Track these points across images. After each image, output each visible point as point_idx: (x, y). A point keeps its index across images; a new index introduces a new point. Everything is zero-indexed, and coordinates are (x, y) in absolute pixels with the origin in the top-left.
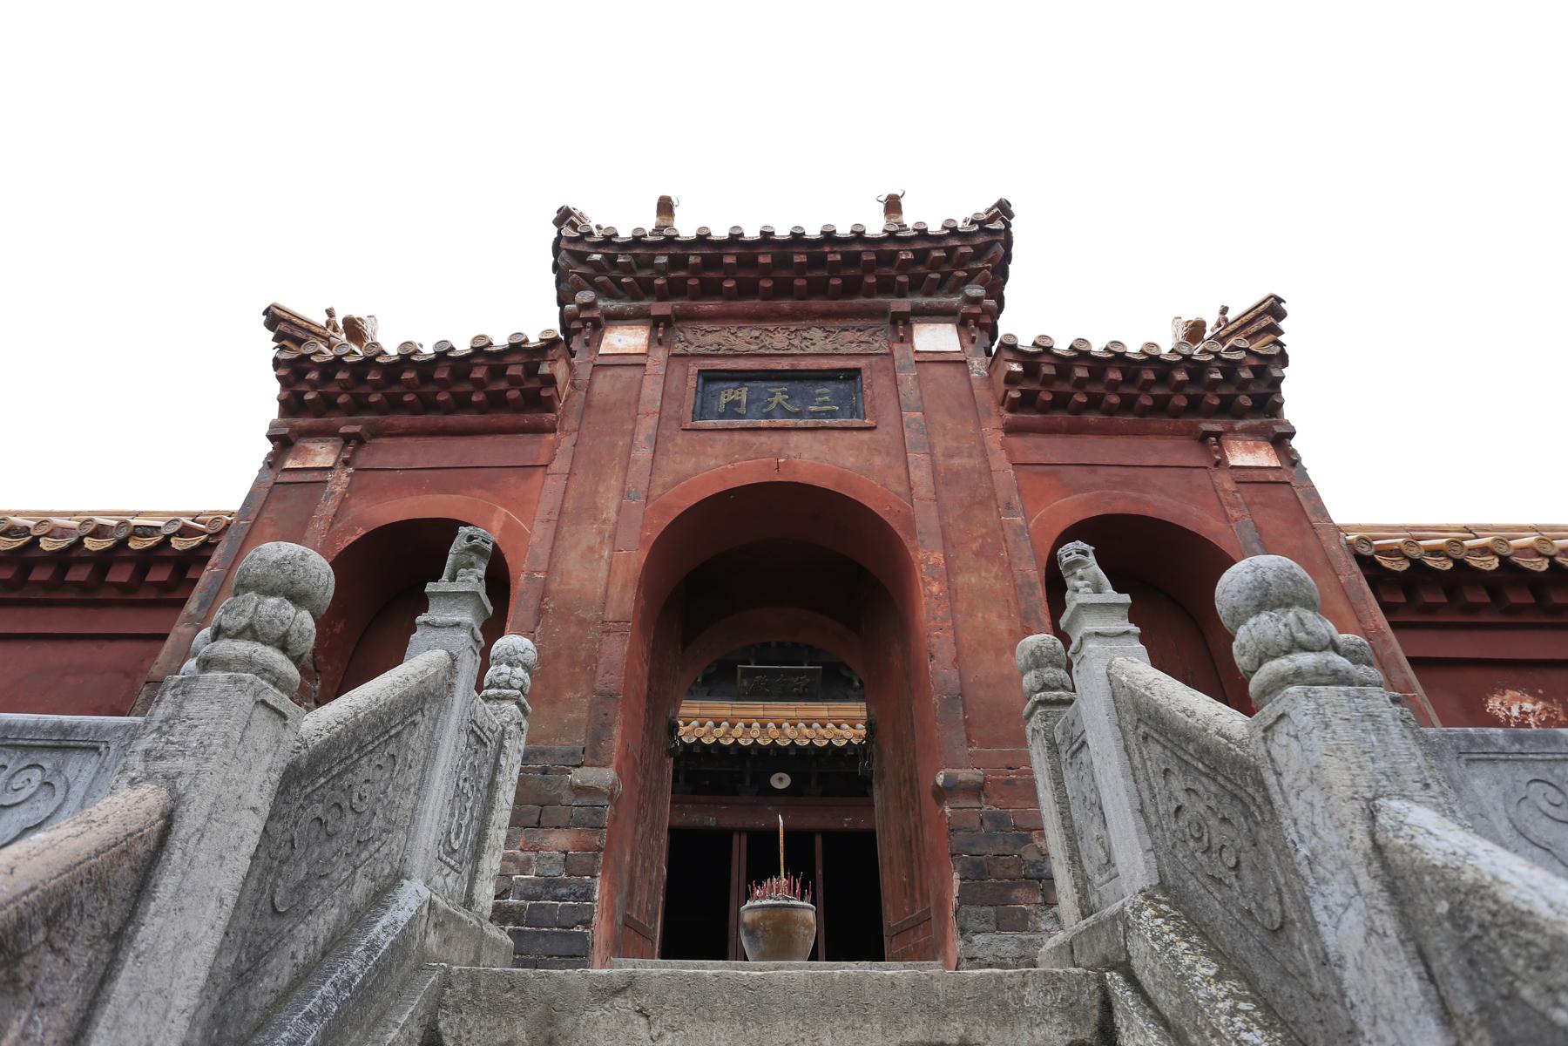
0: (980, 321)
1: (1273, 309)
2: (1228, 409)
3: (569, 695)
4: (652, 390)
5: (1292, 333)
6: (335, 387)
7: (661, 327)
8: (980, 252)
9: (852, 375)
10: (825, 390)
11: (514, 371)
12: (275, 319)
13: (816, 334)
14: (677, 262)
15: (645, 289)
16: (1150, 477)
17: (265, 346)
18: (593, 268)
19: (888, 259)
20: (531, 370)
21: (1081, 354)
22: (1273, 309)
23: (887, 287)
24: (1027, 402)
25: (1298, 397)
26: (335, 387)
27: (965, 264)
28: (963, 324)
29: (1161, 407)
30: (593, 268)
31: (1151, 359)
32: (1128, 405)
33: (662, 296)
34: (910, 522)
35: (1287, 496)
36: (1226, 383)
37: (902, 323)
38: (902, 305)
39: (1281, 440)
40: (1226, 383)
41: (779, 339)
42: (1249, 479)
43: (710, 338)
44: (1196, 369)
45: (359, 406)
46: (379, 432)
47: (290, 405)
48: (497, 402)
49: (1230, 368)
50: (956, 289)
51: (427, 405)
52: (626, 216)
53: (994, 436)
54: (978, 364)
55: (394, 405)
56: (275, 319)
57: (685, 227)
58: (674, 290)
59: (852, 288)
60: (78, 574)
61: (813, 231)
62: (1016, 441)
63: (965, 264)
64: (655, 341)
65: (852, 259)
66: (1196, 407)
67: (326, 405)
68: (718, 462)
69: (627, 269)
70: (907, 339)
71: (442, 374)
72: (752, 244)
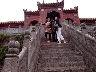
1: (78, 7)
2: (75, 12)
3: (48, 23)
4: (44, 13)
5: (78, 8)
6: (27, 14)
7: (44, 9)
8: (62, 3)
11: (35, 13)
12: (38, 2)
13: (53, 9)
14: (45, 5)
15: (43, 7)
16: (70, 16)
17: (37, 4)
18: (40, 6)
19: (57, 4)
21: (67, 10)
22: (78, 7)
23: (57, 6)
24: (64, 13)
25: (79, 11)
26: (27, 14)
28: (61, 8)
29: (71, 12)
30: (40, 6)
31: (69, 10)
32: (69, 13)
33: (44, 7)
35: (77, 16)
36: (75, 11)
37: (58, 8)
38: (58, 7)
39: (77, 14)
40: (75, 11)
42: (75, 16)
47: (25, 15)
48: (36, 14)
49: (75, 10)
51: (33, 14)
52: (41, 2)
55: (31, 14)
56: (24, 10)
57: (45, 3)
58: (45, 7)
59: (55, 6)
61: (52, 3)
62: (63, 15)
64: (44, 10)
65: (55, 5)
66: (73, 12)
67: (27, 15)
69: (42, 6)
71: (65, 11)
72: (49, 4)
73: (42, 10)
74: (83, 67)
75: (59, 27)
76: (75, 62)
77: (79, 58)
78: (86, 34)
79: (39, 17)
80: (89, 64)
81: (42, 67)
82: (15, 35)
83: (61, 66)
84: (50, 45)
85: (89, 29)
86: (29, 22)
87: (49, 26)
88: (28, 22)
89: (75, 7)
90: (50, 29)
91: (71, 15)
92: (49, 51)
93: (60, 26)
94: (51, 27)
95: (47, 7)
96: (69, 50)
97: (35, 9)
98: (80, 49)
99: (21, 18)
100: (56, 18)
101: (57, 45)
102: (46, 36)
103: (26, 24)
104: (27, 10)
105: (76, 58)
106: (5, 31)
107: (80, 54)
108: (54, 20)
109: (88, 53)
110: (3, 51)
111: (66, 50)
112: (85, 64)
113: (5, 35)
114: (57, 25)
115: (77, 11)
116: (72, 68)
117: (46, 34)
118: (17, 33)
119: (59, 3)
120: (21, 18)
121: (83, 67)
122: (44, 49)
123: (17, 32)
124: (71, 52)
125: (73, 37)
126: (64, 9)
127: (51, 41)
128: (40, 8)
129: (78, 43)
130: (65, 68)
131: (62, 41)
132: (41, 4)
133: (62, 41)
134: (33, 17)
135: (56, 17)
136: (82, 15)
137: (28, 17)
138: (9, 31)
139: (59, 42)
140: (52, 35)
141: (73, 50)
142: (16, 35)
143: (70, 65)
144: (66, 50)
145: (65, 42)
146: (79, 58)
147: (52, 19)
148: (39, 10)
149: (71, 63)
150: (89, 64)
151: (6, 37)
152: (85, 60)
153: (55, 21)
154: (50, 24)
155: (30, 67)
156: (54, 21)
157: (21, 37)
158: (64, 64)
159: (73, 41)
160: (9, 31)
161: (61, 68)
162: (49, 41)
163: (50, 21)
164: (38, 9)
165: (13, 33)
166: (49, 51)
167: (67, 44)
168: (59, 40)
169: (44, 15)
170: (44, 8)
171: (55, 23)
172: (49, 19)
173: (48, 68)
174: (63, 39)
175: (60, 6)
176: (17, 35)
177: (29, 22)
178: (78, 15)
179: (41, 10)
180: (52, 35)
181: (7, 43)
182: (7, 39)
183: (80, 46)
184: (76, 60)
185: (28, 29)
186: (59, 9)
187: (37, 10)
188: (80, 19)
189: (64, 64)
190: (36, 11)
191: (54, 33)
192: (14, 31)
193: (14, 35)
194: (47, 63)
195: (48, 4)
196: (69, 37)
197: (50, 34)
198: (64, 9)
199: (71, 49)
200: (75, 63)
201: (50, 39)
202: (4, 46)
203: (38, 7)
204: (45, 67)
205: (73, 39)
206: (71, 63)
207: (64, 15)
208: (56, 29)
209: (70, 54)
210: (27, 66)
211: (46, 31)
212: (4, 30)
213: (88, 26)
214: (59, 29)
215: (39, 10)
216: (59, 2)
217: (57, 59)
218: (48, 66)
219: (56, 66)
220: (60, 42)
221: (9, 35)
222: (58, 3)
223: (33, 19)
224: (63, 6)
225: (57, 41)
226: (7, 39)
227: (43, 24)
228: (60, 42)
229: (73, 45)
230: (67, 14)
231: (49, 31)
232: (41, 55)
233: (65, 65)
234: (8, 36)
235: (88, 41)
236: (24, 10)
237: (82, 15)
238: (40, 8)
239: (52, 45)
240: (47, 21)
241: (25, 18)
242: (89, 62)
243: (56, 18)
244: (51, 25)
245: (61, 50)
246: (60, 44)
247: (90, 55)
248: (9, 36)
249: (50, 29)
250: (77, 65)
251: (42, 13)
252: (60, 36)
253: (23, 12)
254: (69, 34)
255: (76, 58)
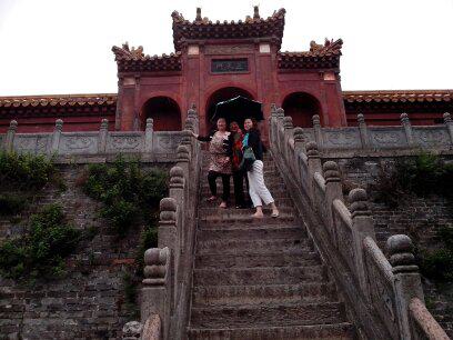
0: (278, 44)
1: (340, 42)
2: (327, 67)
3: (220, 137)
6: (130, 64)
7: (201, 47)
9: (246, 59)
10: (239, 64)
12: (174, 15)
15: (197, 36)
17: (170, 21)
18: (184, 32)
20: (176, 62)
24: (283, 66)
26: (130, 64)
27: (272, 28)
28: (271, 46)
29: (312, 67)
30: (184, 32)
33: (201, 38)
34: (256, 94)
36: (326, 59)
37: (257, 45)
38: (257, 40)
40: (326, 59)
41: (229, 50)
42: (329, 84)
43: (212, 50)
44: (319, 58)
45: (138, 70)
46: (143, 76)
47: (121, 70)
48: (169, 69)
49: (327, 58)
50: (271, 35)
53: (275, 74)
54: (274, 56)
55: (146, 69)
56: (115, 49)
58: (204, 36)
60: (87, 110)
63: (272, 28)
66: (320, 66)
67: (129, 70)
68: (217, 82)
70: (258, 50)
73: (193, 51)
74: (319, 299)
75: (259, 157)
76: (298, 286)
77: (313, 271)
78: (336, 197)
79: (181, 79)
80: (334, 292)
81: (205, 296)
82: (85, 160)
83: (258, 294)
84: (228, 221)
85: (374, 141)
86: (136, 104)
87: (224, 147)
88: (133, 100)
89: (327, 43)
90: (228, 159)
91: (312, 77)
92: (224, 247)
93: (260, 150)
94: (229, 154)
95: (212, 36)
96: (286, 244)
97: (160, 44)
98: (319, 243)
99: (103, 80)
100: (249, 123)
101: (250, 221)
102: (213, 187)
103: (126, 109)
104: (126, 47)
105: (302, 272)
106: (42, 143)
107: (317, 259)
108: (242, 128)
109: (335, 259)
110: (45, 227)
111: (277, 244)
112: (324, 290)
113: (47, 160)
114: (248, 154)
115: (338, 61)
116: (287, 302)
117: (213, 175)
118: (91, 152)
119: (263, 22)
120: (103, 80)
121: (319, 299)
122: (207, 235)
123: (93, 150)
124: (292, 249)
125: (304, 193)
126: (283, 50)
127: (228, 206)
128: (183, 39)
129: (314, 220)
130: (268, 301)
131: (267, 210)
132: (187, 23)
133: (267, 210)
134: (161, 78)
135: (249, 120)
136: (356, 77)
137: (131, 82)
138: (60, 145)
139: (255, 210)
140: (231, 180)
141: (297, 242)
142: (90, 160)
143: (282, 294)
144: (277, 244)
145: (276, 213)
146: (313, 271)
147: (234, 124)
148: (179, 53)
149: (287, 287)
150: (334, 292)
151: (49, 171)
152: (326, 278)
153: (244, 132)
154: (225, 141)
155: (179, 296)
156: (240, 131)
157: (112, 171)
158: (267, 289)
159: (301, 206)
160: (60, 145)
161: (259, 300)
162: (223, 205)
163: (227, 129)
164: (177, 47)
165: (78, 151)
166: (224, 247)
167: (283, 220)
168: (257, 202)
169: (201, 75)
170: (202, 42)
171: (245, 142)
172: (220, 122)
173: (222, 301)
174: (270, 199)
175: (269, 34)
176: (95, 160)
177: (139, 104)
178: (338, 79)
179: (186, 52)
180: (231, 180)
181: (57, 195)
182: (55, 177)
183: (320, 230)
184: (301, 277)
185: (134, 136)
186: (265, 49)
187: (173, 50)
188: (349, 94)
189: (267, 289)
190: (165, 57)
191: (241, 172)
192: (79, 143)
193: (81, 161)
194: (219, 288)
195: (218, 23)
196: (294, 190)
197: (226, 179)
198: (283, 50)
199: (293, 239)
200: (296, 287)
201: (226, 197)
202: (46, 206)
203: (176, 38)
204: (215, 297)
205: (305, 202)
206: (287, 287)
207: (283, 78)
208: (249, 165)
209: (287, 258)
210: (172, 296)
211: (213, 167)
212: (39, 137)
213: (373, 130)
214: (259, 164)
215: (179, 53)
216: (265, 18)
217: (248, 274)
218: (222, 295)
219: (244, 294)
220: (259, 209)
221: (63, 161)
222: (258, 21)
223: (156, 88)
224: (281, 35)
225: (246, 203)
226: (55, 177)
227: (199, 138)
228: (259, 209)
229: (302, 223)
230: (294, 73)
231: (225, 166)
232: (200, 260)
233: (269, 294)
234: (57, 165)
235: (339, 223)
236: (115, 49)
237: (356, 77)
238: (183, 39)
239: (233, 221)
240: (212, 129)
241: (120, 84)
242: (334, 285)
243: (249, 123)
244: (230, 147)
245: (261, 242)
246: (259, 219)
247: (339, 265)
248: (63, 167)
249: (228, 159)
250: (303, 293)
251: (191, 64)
252: (259, 190)
253: (114, 56)
254: (294, 177)
255: (302, 272)
